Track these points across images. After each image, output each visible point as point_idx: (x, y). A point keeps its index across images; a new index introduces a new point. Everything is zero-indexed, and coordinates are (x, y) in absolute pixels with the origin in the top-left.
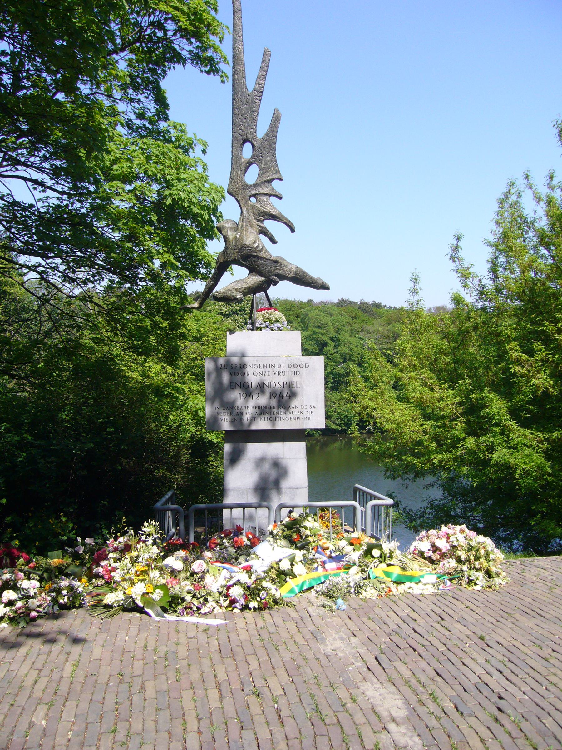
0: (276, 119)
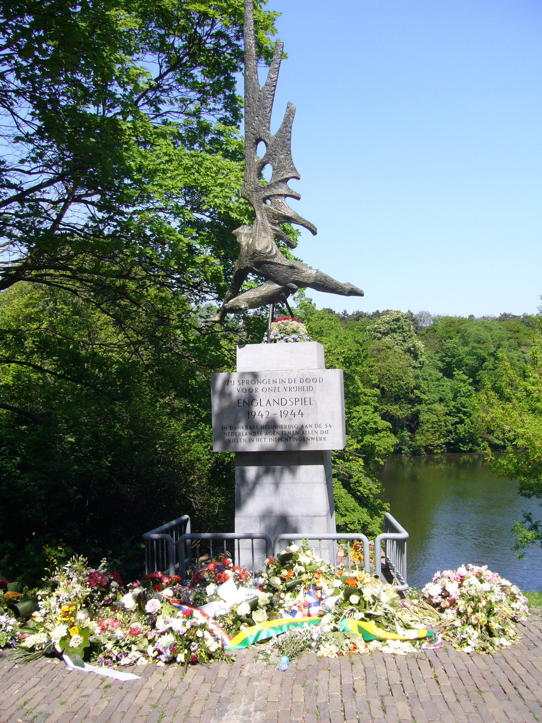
0: (290, 114)
